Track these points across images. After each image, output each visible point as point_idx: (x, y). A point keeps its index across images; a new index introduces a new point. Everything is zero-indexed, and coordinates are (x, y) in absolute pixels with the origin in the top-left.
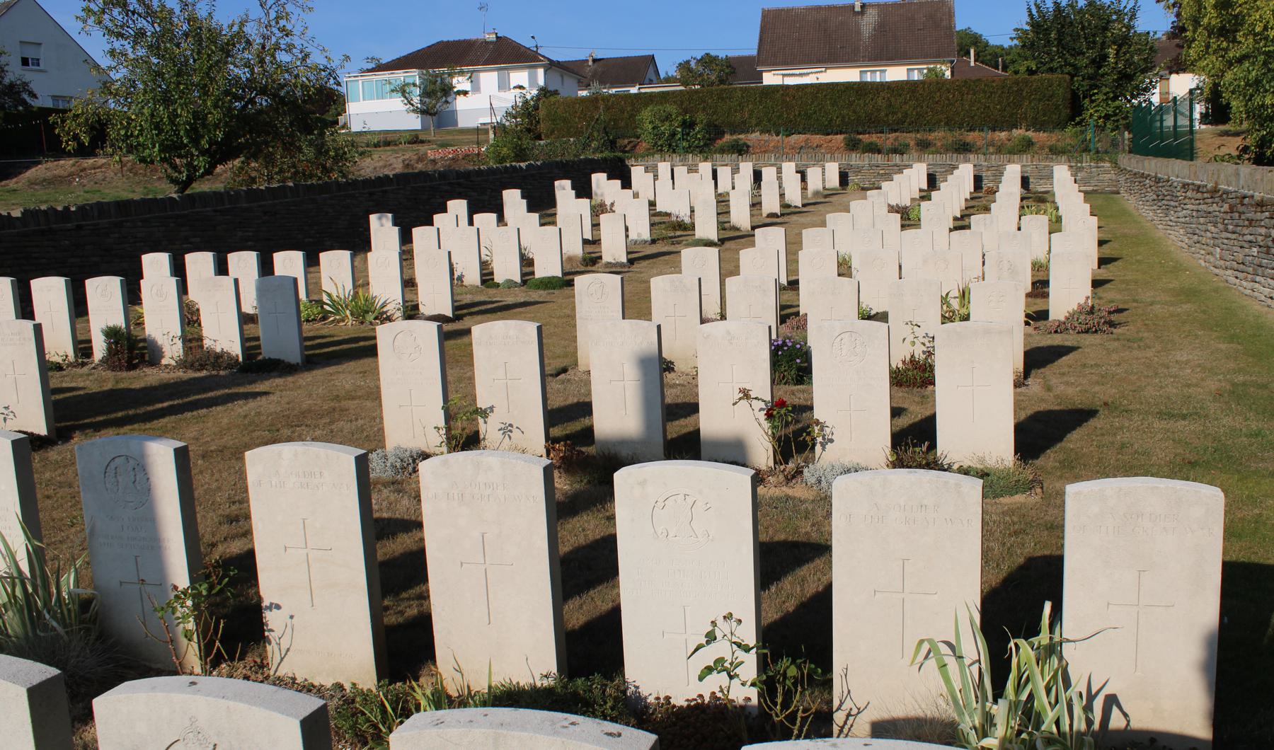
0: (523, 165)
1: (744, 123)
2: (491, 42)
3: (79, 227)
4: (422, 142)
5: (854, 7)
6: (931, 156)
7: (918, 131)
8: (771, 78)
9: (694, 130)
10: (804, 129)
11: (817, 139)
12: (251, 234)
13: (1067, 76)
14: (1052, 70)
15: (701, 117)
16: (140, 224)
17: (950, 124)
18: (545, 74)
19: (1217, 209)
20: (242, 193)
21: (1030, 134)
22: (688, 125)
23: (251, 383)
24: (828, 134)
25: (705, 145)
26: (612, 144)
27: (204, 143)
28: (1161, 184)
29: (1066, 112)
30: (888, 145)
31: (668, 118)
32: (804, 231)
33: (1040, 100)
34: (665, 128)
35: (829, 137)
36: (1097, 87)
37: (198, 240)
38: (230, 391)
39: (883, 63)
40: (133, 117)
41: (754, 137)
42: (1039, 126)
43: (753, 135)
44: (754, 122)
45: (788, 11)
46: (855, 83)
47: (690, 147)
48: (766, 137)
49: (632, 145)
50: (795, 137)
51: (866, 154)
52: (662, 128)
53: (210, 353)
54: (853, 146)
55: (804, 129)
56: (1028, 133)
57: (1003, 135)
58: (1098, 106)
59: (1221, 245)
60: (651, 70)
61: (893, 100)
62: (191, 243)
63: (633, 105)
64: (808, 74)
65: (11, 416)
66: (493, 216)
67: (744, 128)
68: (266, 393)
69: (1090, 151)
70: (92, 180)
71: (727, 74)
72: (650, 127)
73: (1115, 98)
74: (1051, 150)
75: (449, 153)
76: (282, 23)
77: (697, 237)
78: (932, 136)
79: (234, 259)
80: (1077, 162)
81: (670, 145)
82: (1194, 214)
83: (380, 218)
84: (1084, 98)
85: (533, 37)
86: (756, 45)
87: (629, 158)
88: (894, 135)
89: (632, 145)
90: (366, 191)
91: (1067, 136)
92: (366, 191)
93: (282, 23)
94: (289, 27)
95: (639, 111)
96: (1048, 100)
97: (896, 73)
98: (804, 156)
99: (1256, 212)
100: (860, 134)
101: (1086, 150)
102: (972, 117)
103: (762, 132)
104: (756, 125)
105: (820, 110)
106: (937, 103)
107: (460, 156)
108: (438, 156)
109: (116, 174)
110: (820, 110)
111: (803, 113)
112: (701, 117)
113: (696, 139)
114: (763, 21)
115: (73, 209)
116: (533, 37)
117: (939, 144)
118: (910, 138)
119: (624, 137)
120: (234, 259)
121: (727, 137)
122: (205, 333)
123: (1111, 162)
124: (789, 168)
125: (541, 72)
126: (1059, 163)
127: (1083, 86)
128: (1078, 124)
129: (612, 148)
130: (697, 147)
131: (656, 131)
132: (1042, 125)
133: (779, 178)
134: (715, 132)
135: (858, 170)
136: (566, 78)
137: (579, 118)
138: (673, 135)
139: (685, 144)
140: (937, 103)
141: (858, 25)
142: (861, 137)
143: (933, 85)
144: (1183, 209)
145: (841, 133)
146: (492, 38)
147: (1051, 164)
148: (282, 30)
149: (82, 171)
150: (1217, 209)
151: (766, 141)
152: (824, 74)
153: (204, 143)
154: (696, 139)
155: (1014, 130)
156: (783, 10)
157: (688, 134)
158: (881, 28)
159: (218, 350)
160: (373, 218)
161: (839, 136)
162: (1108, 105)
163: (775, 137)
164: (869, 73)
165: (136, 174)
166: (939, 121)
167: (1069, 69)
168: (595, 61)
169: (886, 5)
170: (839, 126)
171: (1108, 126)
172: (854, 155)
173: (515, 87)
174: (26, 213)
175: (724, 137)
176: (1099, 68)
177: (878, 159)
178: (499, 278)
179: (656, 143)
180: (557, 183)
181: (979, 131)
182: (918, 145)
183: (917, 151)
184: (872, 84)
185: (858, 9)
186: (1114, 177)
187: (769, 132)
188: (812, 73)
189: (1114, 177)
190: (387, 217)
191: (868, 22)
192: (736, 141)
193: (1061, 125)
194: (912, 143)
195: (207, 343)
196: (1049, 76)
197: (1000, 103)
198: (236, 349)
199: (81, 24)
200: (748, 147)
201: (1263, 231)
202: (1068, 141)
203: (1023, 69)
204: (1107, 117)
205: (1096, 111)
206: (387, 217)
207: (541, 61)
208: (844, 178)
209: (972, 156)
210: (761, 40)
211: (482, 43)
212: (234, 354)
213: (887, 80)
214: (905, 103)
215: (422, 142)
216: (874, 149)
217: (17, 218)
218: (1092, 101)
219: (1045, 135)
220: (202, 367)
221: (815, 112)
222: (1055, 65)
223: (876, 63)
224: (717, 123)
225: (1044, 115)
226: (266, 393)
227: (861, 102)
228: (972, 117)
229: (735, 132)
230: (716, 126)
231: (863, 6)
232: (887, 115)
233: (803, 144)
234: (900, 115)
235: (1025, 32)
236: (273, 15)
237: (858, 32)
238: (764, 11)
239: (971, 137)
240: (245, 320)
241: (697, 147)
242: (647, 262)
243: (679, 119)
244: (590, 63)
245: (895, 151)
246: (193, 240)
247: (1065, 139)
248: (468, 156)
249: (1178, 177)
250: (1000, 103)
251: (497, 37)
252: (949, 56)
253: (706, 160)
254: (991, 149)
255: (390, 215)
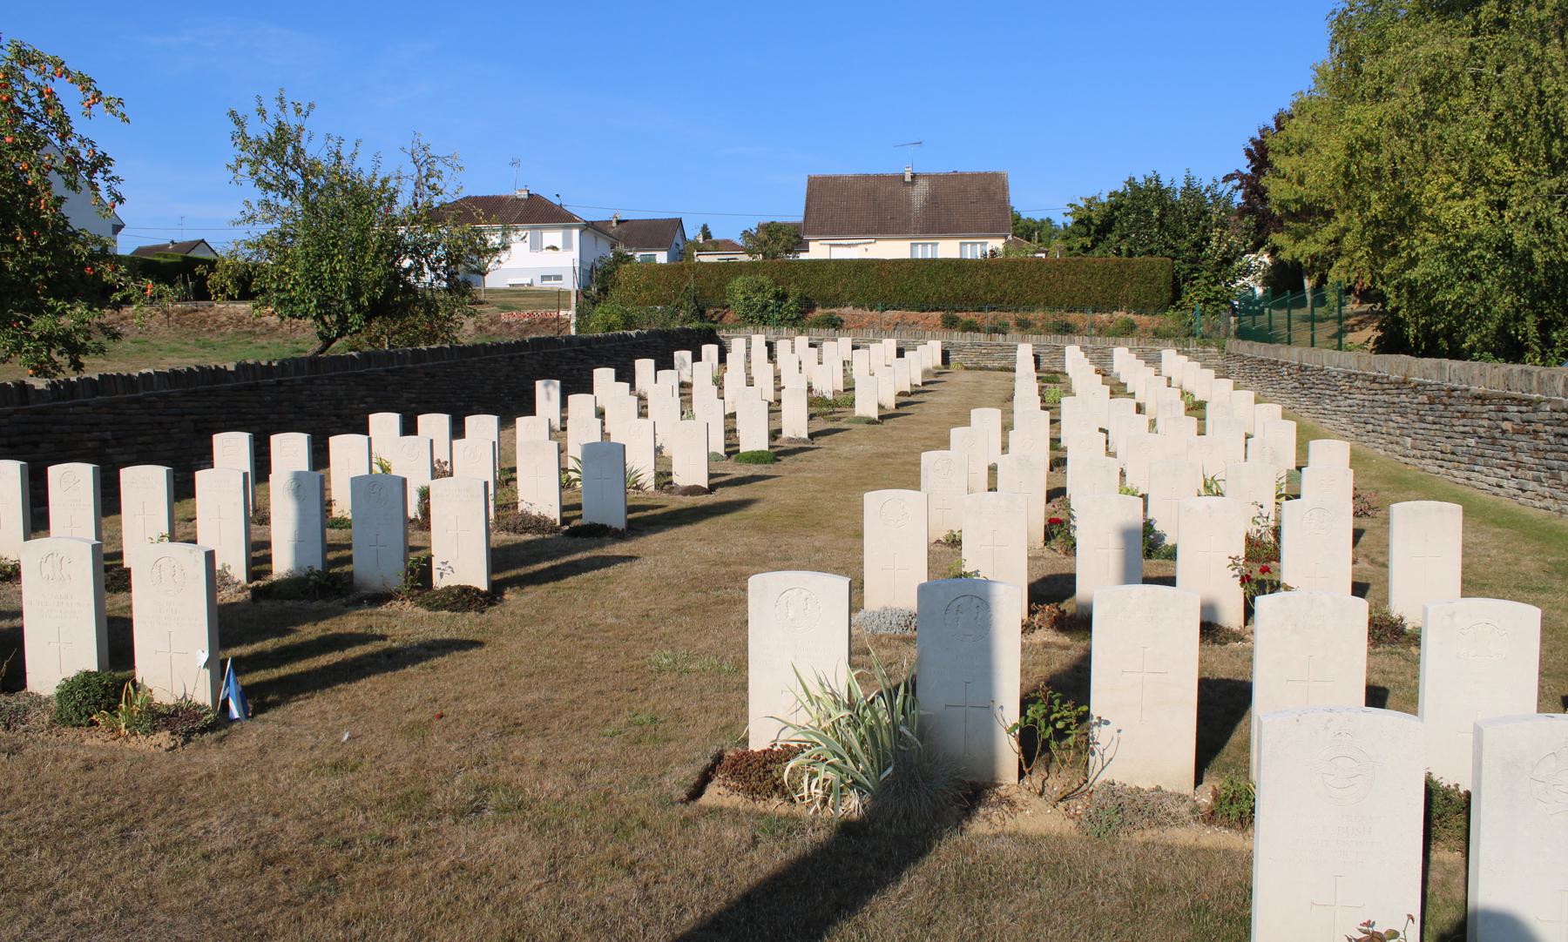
0: (633, 333)
1: (837, 296)
2: (523, 200)
3: (279, 383)
4: (481, 303)
5: (904, 177)
6: (1034, 337)
7: (1017, 311)
8: (818, 250)
9: (786, 302)
10: (899, 305)
11: (913, 315)
12: (414, 396)
13: (1169, 259)
14: (1151, 253)
15: (794, 290)
16: (327, 381)
17: (1050, 304)
18: (580, 235)
19: (1407, 400)
20: (409, 353)
21: (1131, 316)
22: (781, 297)
23: (601, 546)
24: (923, 311)
25: (798, 318)
26: (701, 313)
27: (364, 300)
28: (1308, 373)
29: (1168, 295)
30: (987, 324)
31: (761, 289)
32: (973, 412)
33: (1142, 282)
34: (757, 299)
35: (925, 314)
36: (1197, 270)
37: (371, 399)
38: (593, 554)
39: (936, 235)
40: (287, 270)
41: (847, 312)
42: (1141, 309)
43: (846, 309)
44: (847, 296)
45: (836, 178)
46: (953, 260)
47: (782, 319)
48: (859, 311)
49: (719, 315)
50: (890, 313)
51: (968, 333)
52: (755, 300)
53: (525, 517)
54: (950, 324)
55: (899, 305)
56: (1129, 316)
57: (1105, 317)
58: (1198, 290)
59: (1414, 436)
60: (678, 234)
61: (992, 278)
62: (366, 403)
63: (721, 274)
64: (857, 244)
65: (449, 571)
66: (627, 385)
67: (836, 301)
68: (631, 558)
69: (1195, 335)
70: (135, 330)
71: (794, 244)
72: (742, 297)
73: (1217, 282)
74: (1155, 334)
75: (525, 316)
76: (432, 181)
77: (857, 414)
78: (1031, 316)
79: (424, 421)
80: (1184, 346)
81: (761, 318)
82: (1366, 403)
83: (546, 386)
84: (1184, 281)
85: (558, 195)
86: (803, 213)
87: (719, 329)
88: (992, 314)
89: (719, 315)
90: (507, 355)
91: (1169, 320)
92: (507, 355)
93: (432, 181)
94: (440, 186)
95: (728, 282)
96: (1150, 283)
97: (948, 249)
98: (904, 333)
99: (1472, 405)
100: (956, 311)
101: (1192, 334)
102: (1073, 298)
103: (855, 307)
104: (849, 299)
105: (917, 286)
106: (1037, 282)
107: (537, 321)
108: (512, 319)
109: (161, 324)
110: (917, 286)
111: (898, 288)
112: (794, 290)
113: (789, 311)
114: (809, 188)
115: (274, 364)
116: (558, 195)
117: (1040, 324)
118: (1010, 318)
119: (709, 306)
120: (424, 421)
121: (819, 312)
122: (521, 495)
123: (1218, 347)
124: (759, 341)
125: (576, 232)
126: (1166, 347)
127: (1183, 270)
128: (1178, 307)
129: (701, 318)
130: (789, 320)
131: (747, 302)
132: (1143, 308)
133: (748, 348)
134: (807, 305)
135: (960, 349)
136: (599, 239)
137: (663, 285)
138: (765, 307)
139: (777, 316)
140: (1037, 282)
141: (908, 197)
142: (957, 314)
143: (989, 264)
144: (1347, 398)
145: (937, 310)
146: (524, 195)
147: (1158, 348)
148: (433, 188)
149: (122, 319)
150: (1407, 400)
151: (860, 316)
152: (873, 245)
153: (364, 300)
154: (789, 311)
155: (1115, 312)
156: (830, 178)
157: (780, 306)
158: (933, 200)
159: (535, 513)
160: (539, 384)
161: (934, 313)
162: (1209, 290)
163: (868, 312)
164: (969, 246)
165: (182, 325)
166: (1038, 302)
167: (1168, 252)
168: (619, 222)
169: (937, 176)
170: (935, 303)
171: (1208, 310)
172: (956, 333)
173: (548, 248)
174: (239, 366)
175: (815, 310)
176: (1201, 250)
177: (981, 338)
178: (745, 447)
179: (746, 315)
180: (676, 354)
181: (1081, 312)
182: (1018, 324)
183: (1017, 330)
184: (925, 261)
185: (908, 179)
186: (1221, 362)
187: (862, 307)
188: (857, 244)
189: (1221, 362)
190: (554, 384)
191: (920, 192)
192: (830, 314)
193: (1162, 309)
194: (1012, 323)
195: (522, 507)
196: (1148, 258)
197: (1101, 284)
198: (554, 514)
199: (231, 174)
200: (842, 321)
201: (1486, 423)
202: (1171, 325)
203: (1077, 246)
204: (1207, 301)
205: (1196, 295)
206: (554, 384)
207: (576, 221)
208: (945, 356)
209: (1076, 338)
210: (807, 207)
211: (512, 200)
212: (552, 518)
213: (939, 257)
214: (1005, 282)
215: (481, 303)
216: (971, 327)
217: (231, 372)
218: (1192, 285)
219: (1146, 317)
220: (526, 530)
221: (911, 288)
222: (1154, 246)
223: (922, 236)
224: (808, 296)
225: (1146, 298)
226: (631, 558)
227: (959, 279)
228: (1073, 298)
229: (827, 306)
230: (807, 299)
231: (914, 177)
232: (985, 293)
233: (899, 320)
234: (998, 293)
235: (1078, 209)
236: (424, 173)
237: (909, 203)
238: (810, 178)
239: (1073, 318)
240: (565, 485)
241: (789, 320)
242: (828, 438)
243: (773, 290)
244: (614, 224)
245: (995, 330)
246: (367, 400)
247: (1167, 323)
248: (546, 320)
249: (1338, 366)
250: (1101, 284)
251: (529, 195)
252: (1004, 231)
253: (801, 333)
254: (1093, 331)
255: (558, 383)
